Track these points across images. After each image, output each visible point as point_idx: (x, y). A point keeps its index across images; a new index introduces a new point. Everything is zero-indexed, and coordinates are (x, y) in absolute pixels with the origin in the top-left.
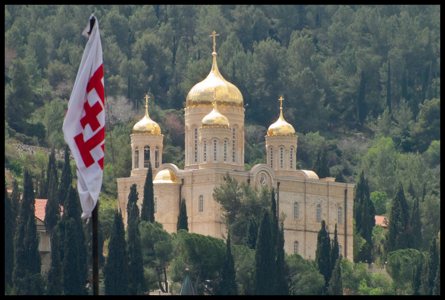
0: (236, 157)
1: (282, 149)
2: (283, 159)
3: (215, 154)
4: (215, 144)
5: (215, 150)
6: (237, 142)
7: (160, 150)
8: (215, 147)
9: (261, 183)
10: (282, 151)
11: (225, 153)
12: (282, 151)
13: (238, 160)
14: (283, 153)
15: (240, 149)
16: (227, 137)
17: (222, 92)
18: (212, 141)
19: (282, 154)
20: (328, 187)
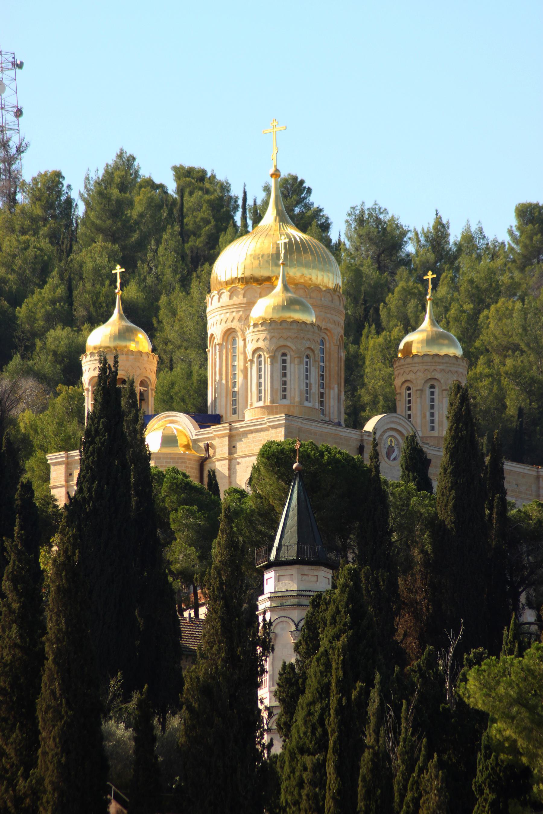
0: (327, 405)
1: (432, 387)
2: (435, 411)
3: (284, 383)
4: (284, 361)
5: (284, 375)
6: (330, 371)
7: (150, 391)
8: (284, 368)
9: (389, 458)
10: (432, 393)
11: (307, 384)
12: (432, 393)
13: (331, 411)
14: (436, 397)
15: (336, 386)
16: (312, 347)
17: (191, 468)
18: (277, 354)
19: (432, 400)
20: (539, 481)
